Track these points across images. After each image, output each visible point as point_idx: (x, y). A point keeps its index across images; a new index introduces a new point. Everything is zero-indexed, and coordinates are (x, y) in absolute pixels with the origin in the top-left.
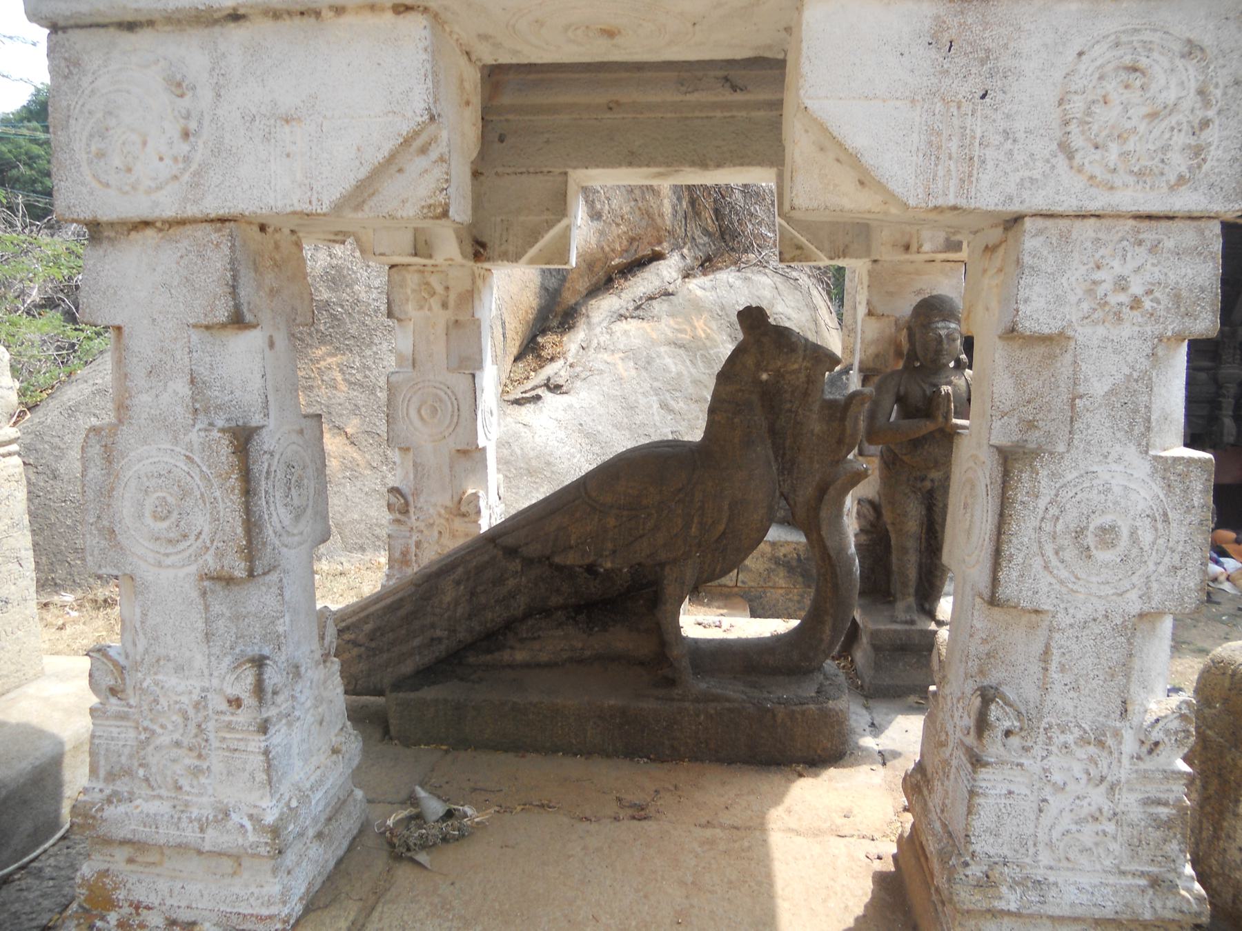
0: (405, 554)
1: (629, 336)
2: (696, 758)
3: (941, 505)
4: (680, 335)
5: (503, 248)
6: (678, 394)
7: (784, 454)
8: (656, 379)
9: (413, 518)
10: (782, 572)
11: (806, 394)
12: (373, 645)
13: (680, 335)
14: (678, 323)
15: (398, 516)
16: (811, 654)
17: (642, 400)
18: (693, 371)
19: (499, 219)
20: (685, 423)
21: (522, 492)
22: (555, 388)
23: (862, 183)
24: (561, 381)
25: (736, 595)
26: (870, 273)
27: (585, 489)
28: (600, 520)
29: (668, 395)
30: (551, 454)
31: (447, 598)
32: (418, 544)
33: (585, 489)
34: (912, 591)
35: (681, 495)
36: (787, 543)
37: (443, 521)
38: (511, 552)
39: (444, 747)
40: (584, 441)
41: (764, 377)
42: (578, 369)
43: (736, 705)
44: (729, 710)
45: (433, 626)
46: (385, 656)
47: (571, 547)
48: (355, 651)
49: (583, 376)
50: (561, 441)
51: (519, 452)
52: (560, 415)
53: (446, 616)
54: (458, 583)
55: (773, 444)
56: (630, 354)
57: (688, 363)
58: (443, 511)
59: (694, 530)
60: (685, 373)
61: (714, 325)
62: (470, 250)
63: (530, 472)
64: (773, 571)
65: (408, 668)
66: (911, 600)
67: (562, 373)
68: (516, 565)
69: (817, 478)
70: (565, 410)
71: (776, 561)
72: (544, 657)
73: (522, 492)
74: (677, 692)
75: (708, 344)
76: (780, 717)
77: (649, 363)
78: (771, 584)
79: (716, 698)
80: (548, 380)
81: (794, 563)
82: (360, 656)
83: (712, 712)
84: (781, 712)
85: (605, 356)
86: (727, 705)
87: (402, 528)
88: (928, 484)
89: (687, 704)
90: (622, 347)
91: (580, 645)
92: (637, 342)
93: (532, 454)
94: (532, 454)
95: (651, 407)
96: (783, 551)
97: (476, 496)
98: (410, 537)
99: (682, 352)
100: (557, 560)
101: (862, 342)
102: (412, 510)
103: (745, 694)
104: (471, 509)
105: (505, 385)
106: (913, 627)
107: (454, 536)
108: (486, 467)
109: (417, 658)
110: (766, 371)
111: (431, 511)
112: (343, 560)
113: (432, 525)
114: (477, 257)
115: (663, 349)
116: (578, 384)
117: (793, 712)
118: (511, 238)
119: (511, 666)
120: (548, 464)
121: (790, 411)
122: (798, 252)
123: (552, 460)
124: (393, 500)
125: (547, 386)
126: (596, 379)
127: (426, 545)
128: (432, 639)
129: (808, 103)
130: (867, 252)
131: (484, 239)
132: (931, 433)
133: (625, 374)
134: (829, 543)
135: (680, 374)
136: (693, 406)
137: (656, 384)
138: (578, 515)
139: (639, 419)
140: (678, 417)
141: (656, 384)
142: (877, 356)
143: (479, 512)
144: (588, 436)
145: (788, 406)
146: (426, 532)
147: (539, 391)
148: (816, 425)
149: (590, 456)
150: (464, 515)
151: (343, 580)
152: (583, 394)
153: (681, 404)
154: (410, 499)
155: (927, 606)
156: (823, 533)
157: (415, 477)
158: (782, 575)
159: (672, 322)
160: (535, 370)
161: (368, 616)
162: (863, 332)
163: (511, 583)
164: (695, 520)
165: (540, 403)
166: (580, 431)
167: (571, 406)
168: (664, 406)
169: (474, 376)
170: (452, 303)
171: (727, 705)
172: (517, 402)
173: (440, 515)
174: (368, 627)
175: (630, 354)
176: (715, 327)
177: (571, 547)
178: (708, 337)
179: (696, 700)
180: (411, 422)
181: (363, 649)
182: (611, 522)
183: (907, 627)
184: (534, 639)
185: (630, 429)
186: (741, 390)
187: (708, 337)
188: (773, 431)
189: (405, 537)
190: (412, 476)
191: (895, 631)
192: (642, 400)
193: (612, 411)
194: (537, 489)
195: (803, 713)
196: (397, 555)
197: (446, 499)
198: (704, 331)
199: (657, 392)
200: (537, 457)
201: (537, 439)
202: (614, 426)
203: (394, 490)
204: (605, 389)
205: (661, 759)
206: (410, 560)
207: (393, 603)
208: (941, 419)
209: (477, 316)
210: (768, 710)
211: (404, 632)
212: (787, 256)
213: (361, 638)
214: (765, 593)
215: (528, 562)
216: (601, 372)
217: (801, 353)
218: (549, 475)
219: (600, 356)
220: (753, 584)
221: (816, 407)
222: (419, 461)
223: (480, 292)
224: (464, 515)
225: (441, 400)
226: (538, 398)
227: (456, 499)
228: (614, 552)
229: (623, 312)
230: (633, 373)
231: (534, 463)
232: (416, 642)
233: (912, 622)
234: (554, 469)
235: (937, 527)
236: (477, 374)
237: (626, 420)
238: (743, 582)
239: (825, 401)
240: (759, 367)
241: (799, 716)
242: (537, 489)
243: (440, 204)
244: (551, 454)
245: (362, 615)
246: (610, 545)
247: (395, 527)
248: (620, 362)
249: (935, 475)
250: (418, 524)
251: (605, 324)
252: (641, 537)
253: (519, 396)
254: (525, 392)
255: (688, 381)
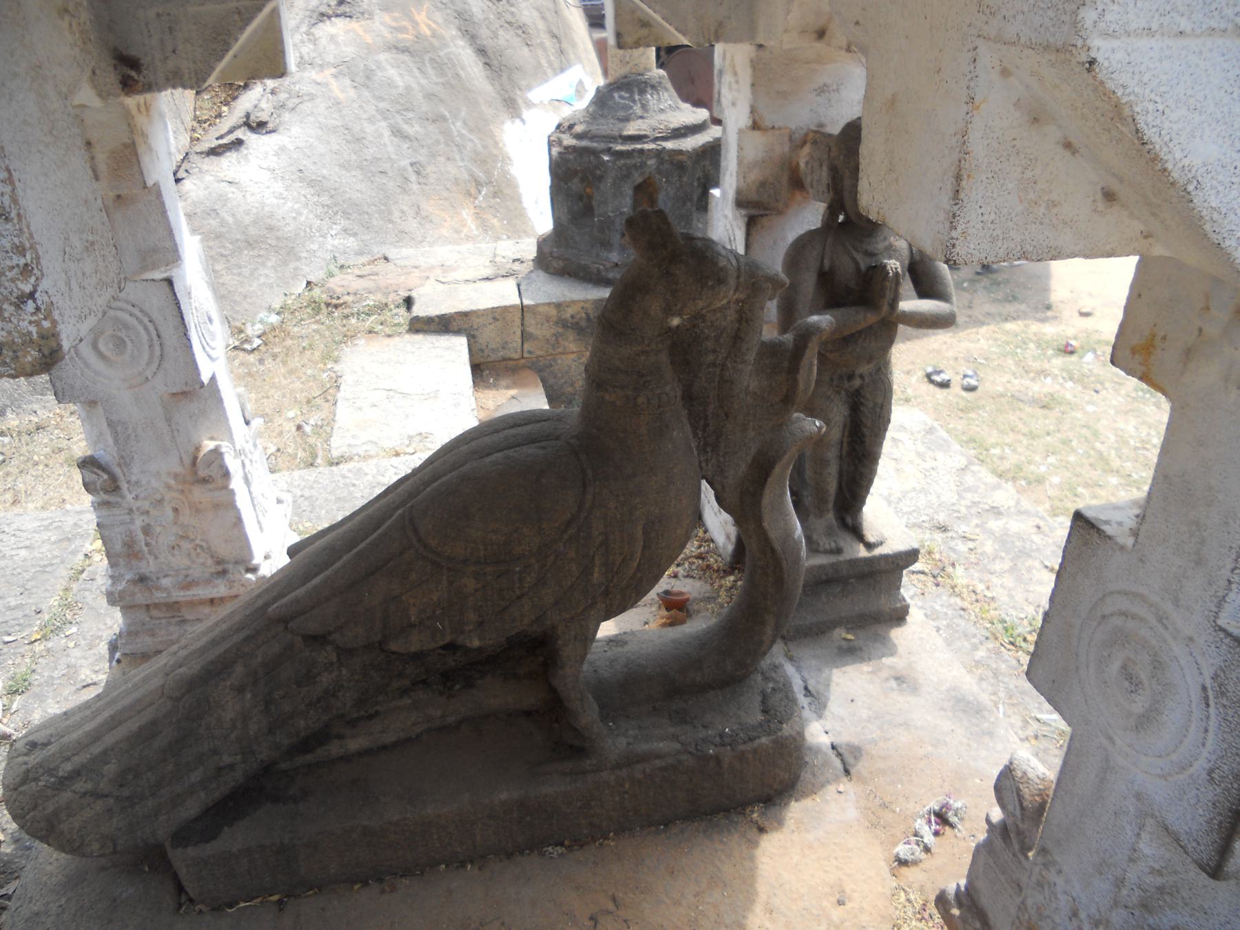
0: (130, 544)
1: (337, 44)
2: (623, 829)
3: (871, 405)
4: (401, 36)
5: (171, 64)
6: (410, 115)
7: (706, 425)
8: (381, 99)
9: (130, 497)
10: (571, 335)
11: (737, 338)
12: (126, 792)
13: (401, 36)
14: (395, 19)
15: (106, 497)
16: (749, 661)
17: (369, 129)
18: (424, 82)
19: (151, 14)
20: (424, 151)
21: (246, 271)
22: (259, 127)
23: (1109, 196)
24: (264, 117)
25: (524, 367)
26: (754, 64)
27: (415, 530)
28: (451, 583)
29: (399, 118)
30: (271, 216)
31: (229, 715)
32: (147, 530)
33: (415, 530)
34: (831, 505)
35: (572, 531)
36: (574, 302)
37: (176, 495)
38: (318, 640)
39: (275, 898)
40: (308, 191)
41: (676, 321)
42: (283, 96)
43: (670, 761)
44: (663, 769)
45: (215, 752)
46: (150, 803)
47: (412, 626)
48: (99, 806)
49: (290, 104)
50: (280, 196)
51: (230, 220)
52: (273, 162)
53: (233, 736)
54: (240, 690)
55: (690, 414)
56: (344, 68)
57: (415, 70)
58: (172, 482)
59: (596, 576)
60: (414, 85)
61: (438, 17)
62: (111, 78)
63: (251, 244)
64: (561, 335)
65: (192, 808)
66: (830, 516)
67: (263, 105)
68: (327, 655)
69: (753, 450)
70: (277, 154)
71: (563, 323)
72: (389, 738)
73: (246, 271)
74: (588, 764)
75: (436, 42)
76: (726, 761)
77: (368, 78)
78: (560, 350)
79: (643, 758)
80: (248, 116)
81: (583, 324)
82: (110, 810)
83: (640, 776)
84: (727, 754)
85: (313, 74)
86: (658, 763)
87: (116, 511)
88: (857, 382)
89: (605, 775)
90: (330, 58)
91: (439, 713)
92: (349, 51)
93: (247, 220)
94: (247, 220)
95: (381, 136)
96: (570, 311)
97: (217, 453)
98: (132, 522)
99: (406, 57)
100: (393, 646)
101: (740, 163)
102: (124, 486)
103: (675, 738)
104: (214, 471)
105: (194, 130)
106: (841, 558)
107: (198, 511)
108: (221, 400)
109: (203, 795)
110: (680, 315)
111: (154, 483)
112: (36, 407)
113: (161, 501)
114: (128, 85)
115: (383, 57)
116: (287, 116)
117: (743, 752)
118: (181, 47)
119: (346, 759)
120: (271, 228)
121: (714, 364)
122: (644, 32)
123: (273, 223)
124: (91, 477)
125: (247, 124)
126: (307, 107)
127: (158, 529)
128: (220, 769)
129: (1101, 48)
130: (748, 32)
131: (133, 52)
132: (870, 327)
133: (341, 96)
134: (772, 535)
135: (408, 88)
136: (431, 128)
137: (382, 105)
138: (414, 576)
139: (371, 152)
140: (415, 144)
141: (382, 105)
142: (763, 184)
143: (226, 475)
144: (311, 183)
145: (711, 357)
146: (153, 512)
147: (239, 134)
148: (748, 379)
149: (320, 210)
150: (205, 481)
151: (42, 438)
152: (296, 130)
153: (417, 128)
154: (117, 471)
155: (849, 521)
156: (765, 525)
157: (116, 441)
158: (571, 338)
159: (387, 19)
160: (227, 104)
161: (105, 753)
162: (740, 148)
163: (326, 679)
164: (597, 562)
165: (243, 150)
166: (302, 180)
167: (283, 148)
168: (397, 132)
169: (169, 282)
170: (103, 168)
171: (658, 763)
172: (214, 152)
173: (169, 487)
174: (111, 769)
175: (344, 68)
176: (440, 20)
177: (412, 626)
178: (434, 35)
179: (618, 766)
180: (87, 365)
181: (111, 801)
182: (470, 584)
183: (832, 559)
184: (370, 717)
185: (361, 168)
186: (644, 352)
187: (434, 35)
188: (689, 397)
189: (123, 523)
190: (110, 441)
191: (821, 567)
192: (369, 129)
193: (335, 147)
194: (263, 264)
195: (755, 751)
196: (118, 547)
197: (173, 464)
198: (429, 27)
199: (384, 114)
200: (255, 222)
201: (250, 199)
202: (342, 166)
203: (87, 464)
204: (321, 119)
205: (578, 843)
206: (141, 551)
207: (141, 729)
208: (885, 308)
209: (150, 183)
210: (711, 757)
211: (170, 767)
212: (629, 39)
213: (103, 786)
214: (555, 360)
215: (346, 652)
216: (312, 97)
217: (732, 282)
218: (274, 242)
219: (306, 74)
220: (541, 353)
221: (751, 357)
222: (115, 417)
223: (144, 135)
224: (205, 481)
225: (126, 327)
226: (239, 143)
227: (187, 460)
228: (481, 624)
229: (323, 9)
230: (352, 93)
231: (253, 231)
232: (196, 776)
233: (839, 551)
234: (279, 234)
235: (866, 432)
236: (174, 273)
237: (354, 157)
238: (530, 352)
239: (763, 344)
240: (668, 311)
241: (750, 756)
242: (263, 264)
243: (28, 341)
244: (271, 216)
245: (96, 749)
246: (472, 616)
247: (105, 512)
248: (332, 81)
249: (865, 369)
250: (139, 504)
251: (304, 29)
252: (519, 598)
253: (215, 143)
254: (221, 137)
255: (420, 96)
